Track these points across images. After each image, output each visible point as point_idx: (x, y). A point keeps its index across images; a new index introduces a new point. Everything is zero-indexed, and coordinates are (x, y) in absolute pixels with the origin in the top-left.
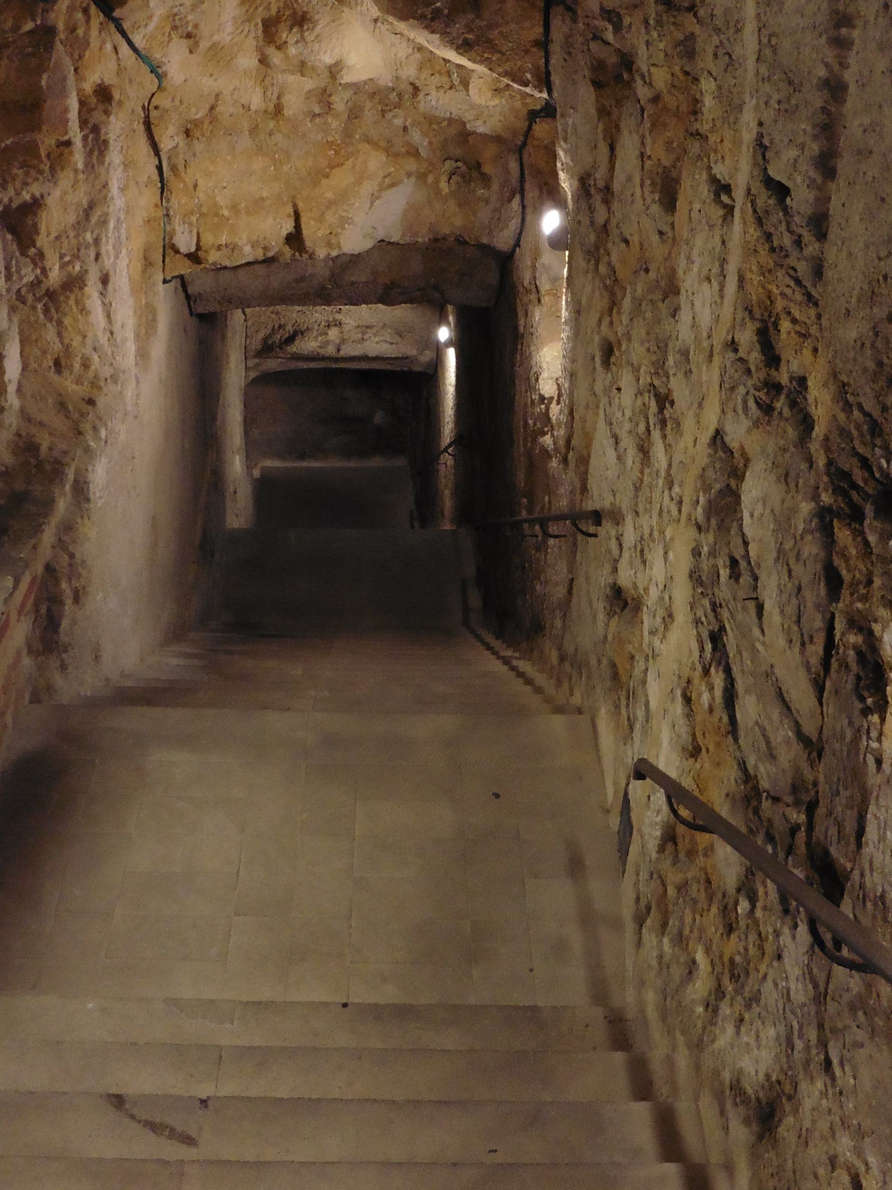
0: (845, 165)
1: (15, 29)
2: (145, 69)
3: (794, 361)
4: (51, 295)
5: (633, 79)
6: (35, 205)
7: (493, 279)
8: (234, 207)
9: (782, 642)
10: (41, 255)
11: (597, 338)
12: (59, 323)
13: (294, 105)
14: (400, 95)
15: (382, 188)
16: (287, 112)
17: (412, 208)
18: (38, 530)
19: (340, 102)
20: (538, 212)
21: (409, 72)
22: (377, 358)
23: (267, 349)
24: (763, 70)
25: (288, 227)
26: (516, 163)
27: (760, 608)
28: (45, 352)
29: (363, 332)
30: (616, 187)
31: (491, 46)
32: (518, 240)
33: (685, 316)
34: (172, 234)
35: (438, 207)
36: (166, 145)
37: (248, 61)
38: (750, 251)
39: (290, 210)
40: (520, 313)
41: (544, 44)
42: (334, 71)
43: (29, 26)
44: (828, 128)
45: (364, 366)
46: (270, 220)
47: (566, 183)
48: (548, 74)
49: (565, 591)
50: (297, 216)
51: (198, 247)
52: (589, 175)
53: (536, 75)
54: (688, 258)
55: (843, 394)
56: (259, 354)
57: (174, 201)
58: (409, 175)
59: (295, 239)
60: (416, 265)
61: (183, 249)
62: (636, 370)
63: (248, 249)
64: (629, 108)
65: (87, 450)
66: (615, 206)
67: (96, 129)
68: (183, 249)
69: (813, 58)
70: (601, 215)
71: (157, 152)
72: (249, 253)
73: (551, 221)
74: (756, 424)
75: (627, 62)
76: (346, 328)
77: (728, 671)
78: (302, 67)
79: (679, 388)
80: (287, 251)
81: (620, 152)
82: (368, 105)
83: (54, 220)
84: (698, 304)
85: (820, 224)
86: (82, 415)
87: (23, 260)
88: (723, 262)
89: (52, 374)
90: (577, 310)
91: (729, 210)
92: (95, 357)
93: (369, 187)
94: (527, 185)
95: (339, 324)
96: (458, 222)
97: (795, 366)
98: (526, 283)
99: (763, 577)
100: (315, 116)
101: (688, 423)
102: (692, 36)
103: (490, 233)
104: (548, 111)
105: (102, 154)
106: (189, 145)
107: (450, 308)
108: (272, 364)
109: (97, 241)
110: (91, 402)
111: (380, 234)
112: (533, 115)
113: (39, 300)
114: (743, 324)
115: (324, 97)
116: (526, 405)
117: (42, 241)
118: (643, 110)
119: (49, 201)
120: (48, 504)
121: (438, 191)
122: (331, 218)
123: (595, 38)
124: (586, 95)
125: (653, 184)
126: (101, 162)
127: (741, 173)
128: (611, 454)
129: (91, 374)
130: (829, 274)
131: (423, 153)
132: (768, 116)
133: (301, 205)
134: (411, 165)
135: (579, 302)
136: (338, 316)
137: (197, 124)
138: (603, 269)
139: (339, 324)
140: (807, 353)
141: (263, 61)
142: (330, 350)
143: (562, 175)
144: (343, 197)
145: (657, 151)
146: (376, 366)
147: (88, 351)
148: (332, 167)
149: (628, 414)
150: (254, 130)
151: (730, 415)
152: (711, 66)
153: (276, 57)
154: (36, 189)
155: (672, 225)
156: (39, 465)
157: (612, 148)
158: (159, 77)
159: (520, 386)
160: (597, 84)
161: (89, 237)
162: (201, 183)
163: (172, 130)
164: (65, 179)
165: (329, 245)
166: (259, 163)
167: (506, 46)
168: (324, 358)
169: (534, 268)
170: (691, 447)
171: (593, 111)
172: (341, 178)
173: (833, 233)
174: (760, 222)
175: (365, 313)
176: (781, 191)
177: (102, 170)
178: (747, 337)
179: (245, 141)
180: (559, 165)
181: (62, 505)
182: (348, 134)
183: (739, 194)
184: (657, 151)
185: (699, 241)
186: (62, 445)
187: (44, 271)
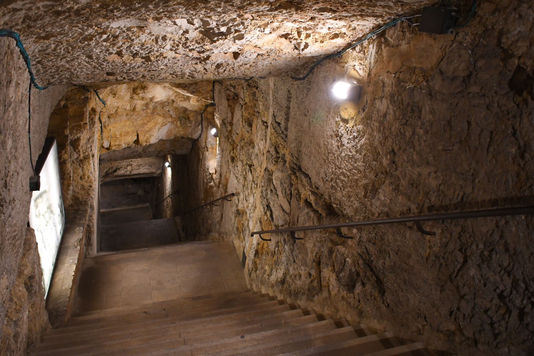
0: (290, 120)
1: (79, 98)
2: (101, 103)
3: (282, 152)
4: (81, 161)
5: (238, 99)
6: (78, 139)
7: (190, 146)
8: (121, 135)
9: (282, 198)
10: (79, 151)
11: (229, 156)
12: (83, 167)
13: (139, 108)
14: (168, 103)
15: (162, 126)
16: (137, 110)
17: (169, 131)
18: (85, 216)
19: (151, 106)
20: (211, 129)
21: (173, 98)
22: (143, 174)
23: (107, 175)
24: (274, 103)
25: (136, 138)
26: (205, 117)
27: (278, 195)
28: (78, 175)
29: (140, 167)
30: (234, 122)
31: (200, 92)
32: (200, 135)
33: (256, 147)
34: (103, 143)
35: (177, 129)
36: (103, 121)
37: (127, 97)
38: (272, 134)
39: (136, 134)
40: (200, 153)
41: (213, 91)
42: (152, 99)
43: (83, 97)
44: (287, 114)
45: (138, 176)
46: (131, 137)
47: (218, 122)
48: (214, 97)
49: (220, 218)
50: (138, 135)
51: (110, 146)
52: (225, 119)
53: (211, 98)
54: (257, 136)
55: (292, 155)
56: (104, 177)
57: (104, 134)
58: (169, 122)
59: (137, 142)
60: (168, 145)
61: (106, 147)
62: (242, 161)
63: (124, 145)
64: (238, 105)
65: (92, 198)
66: (234, 126)
67: (92, 119)
68: (106, 147)
69: (284, 103)
70: (229, 128)
71: (101, 123)
72: (124, 146)
73: (213, 131)
74: (274, 165)
75: (237, 95)
76: (133, 166)
77: (271, 211)
78: (143, 99)
79: (255, 162)
80: (134, 145)
81: (235, 115)
82: (159, 106)
83: (83, 142)
84: (260, 145)
85: (286, 129)
86: (89, 190)
87: (74, 153)
88: (266, 136)
89: (79, 180)
90: (222, 151)
91: (267, 127)
92: (91, 175)
93: (158, 126)
94: (203, 122)
95: (131, 165)
96: (182, 133)
97: (282, 153)
98: (203, 146)
99: (278, 190)
100: (144, 110)
101: (258, 169)
102: (255, 92)
103: (192, 135)
104: (213, 105)
105: (94, 125)
106: (109, 120)
107: (169, 156)
108: (108, 179)
109: (91, 147)
110: (91, 186)
111: (160, 138)
112: (207, 106)
113: (77, 162)
114: (271, 147)
115: (147, 105)
116: (204, 177)
117: (80, 148)
118: (242, 106)
119: (81, 138)
120: (86, 211)
121: (177, 125)
122: (147, 135)
123: (228, 90)
124: (225, 103)
125: (245, 121)
126: (93, 127)
127: (270, 121)
128: (235, 181)
129: (90, 180)
130: (288, 136)
131: (173, 116)
132: (276, 111)
133: (139, 133)
134: (170, 120)
135: (223, 149)
136: (131, 163)
137: (112, 115)
138: (230, 140)
139: (131, 165)
140: (285, 150)
141: (132, 98)
142: (128, 173)
143: (216, 120)
144: (150, 130)
145: (246, 114)
146: (142, 176)
147: (89, 174)
148: (148, 122)
149: (240, 171)
150: (127, 115)
151: (269, 164)
152: (261, 99)
153: (135, 97)
154: (78, 135)
155: (251, 130)
156: (81, 203)
157: (232, 114)
158: (105, 104)
159: (201, 173)
160: (228, 100)
161: (89, 146)
162: (112, 129)
163: (105, 117)
164: (85, 132)
165: (147, 142)
166: (128, 123)
167: (203, 92)
168: (126, 176)
169: (206, 142)
170: (259, 171)
171: (227, 106)
172: (150, 125)
173: (289, 130)
174: (274, 129)
175: (139, 161)
176: (279, 124)
177: (93, 129)
178: (272, 150)
179: (124, 118)
180: (215, 117)
181: (89, 210)
182: (153, 113)
183: (269, 124)
184: (246, 114)
185: (259, 133)
186: (85, 197)
187: (80, 155)
